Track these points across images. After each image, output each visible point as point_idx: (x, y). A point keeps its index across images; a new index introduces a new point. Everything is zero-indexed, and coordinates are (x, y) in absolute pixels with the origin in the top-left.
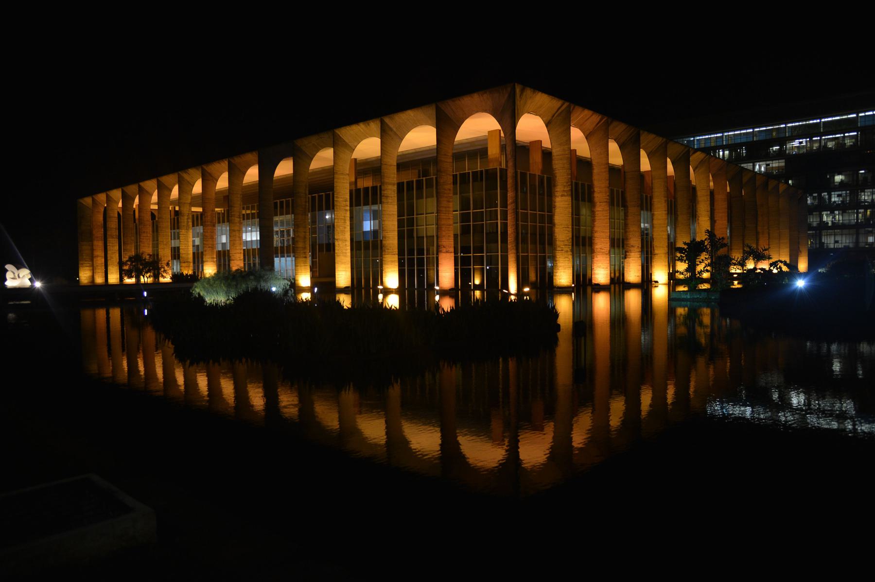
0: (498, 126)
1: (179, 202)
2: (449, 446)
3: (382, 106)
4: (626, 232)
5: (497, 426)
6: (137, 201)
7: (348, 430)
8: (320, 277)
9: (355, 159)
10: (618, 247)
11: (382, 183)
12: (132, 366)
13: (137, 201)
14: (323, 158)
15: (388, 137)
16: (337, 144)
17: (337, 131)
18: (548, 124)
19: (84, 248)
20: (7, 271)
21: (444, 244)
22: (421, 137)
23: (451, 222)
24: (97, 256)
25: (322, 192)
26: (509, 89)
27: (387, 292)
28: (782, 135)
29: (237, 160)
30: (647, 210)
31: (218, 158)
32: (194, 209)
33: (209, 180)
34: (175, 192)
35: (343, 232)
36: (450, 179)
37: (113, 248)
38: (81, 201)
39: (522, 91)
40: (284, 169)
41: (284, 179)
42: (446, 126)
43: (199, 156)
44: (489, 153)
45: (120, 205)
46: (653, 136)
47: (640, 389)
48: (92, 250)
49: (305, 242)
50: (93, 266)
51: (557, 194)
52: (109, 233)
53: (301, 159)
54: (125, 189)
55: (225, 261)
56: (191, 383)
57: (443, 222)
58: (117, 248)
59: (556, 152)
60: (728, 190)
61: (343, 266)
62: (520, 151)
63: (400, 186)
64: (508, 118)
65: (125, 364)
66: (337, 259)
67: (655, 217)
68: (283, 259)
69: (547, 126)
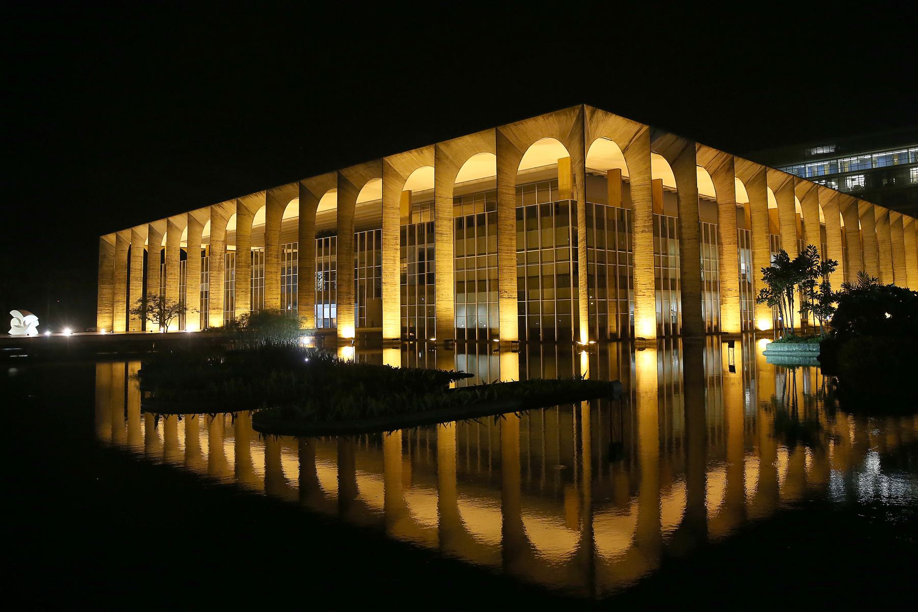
0: (566, 154)
1: (211, 240)
3: (434, 128)
4: (721, 273)
5: (571, 505)
7: (395, 510)
9: (410, 191)
10: (666, 288)
11: (437, 218)
16: (384, 173)
17: (387, 159)
19: (104, 291)
21: (506, 288)
22: (478, 165)
23: (514, 263)
25: (370, 231)
26: (577, 111)
28: (904, 162)
29: (277, 192)
30: (748, 247)
33: (308, 203)
34: (207, 231)
35: (393, 274)
36: (513, 214)
38: (103, 237)
39: (593, 113)
41: (326, 215)
42: (508, 153)
43: (234, 188)
44: (560, 184)
45: (147, 243)
46: (750, 163)
47: (744, 463)
48: (114, 294)
49: (349, 286)
51: (638, 230)
53: (347, 192)
55: (412, 302)
56: (216, 452)
57: (505, 263)
59: (634, 182)
60: (842, 224)
62: (594, 181)
63: (459, 223)
64: (579, 141)
65: (143, 428)
67: (756, 256)
68: (320, 306)
69: (623, 152)
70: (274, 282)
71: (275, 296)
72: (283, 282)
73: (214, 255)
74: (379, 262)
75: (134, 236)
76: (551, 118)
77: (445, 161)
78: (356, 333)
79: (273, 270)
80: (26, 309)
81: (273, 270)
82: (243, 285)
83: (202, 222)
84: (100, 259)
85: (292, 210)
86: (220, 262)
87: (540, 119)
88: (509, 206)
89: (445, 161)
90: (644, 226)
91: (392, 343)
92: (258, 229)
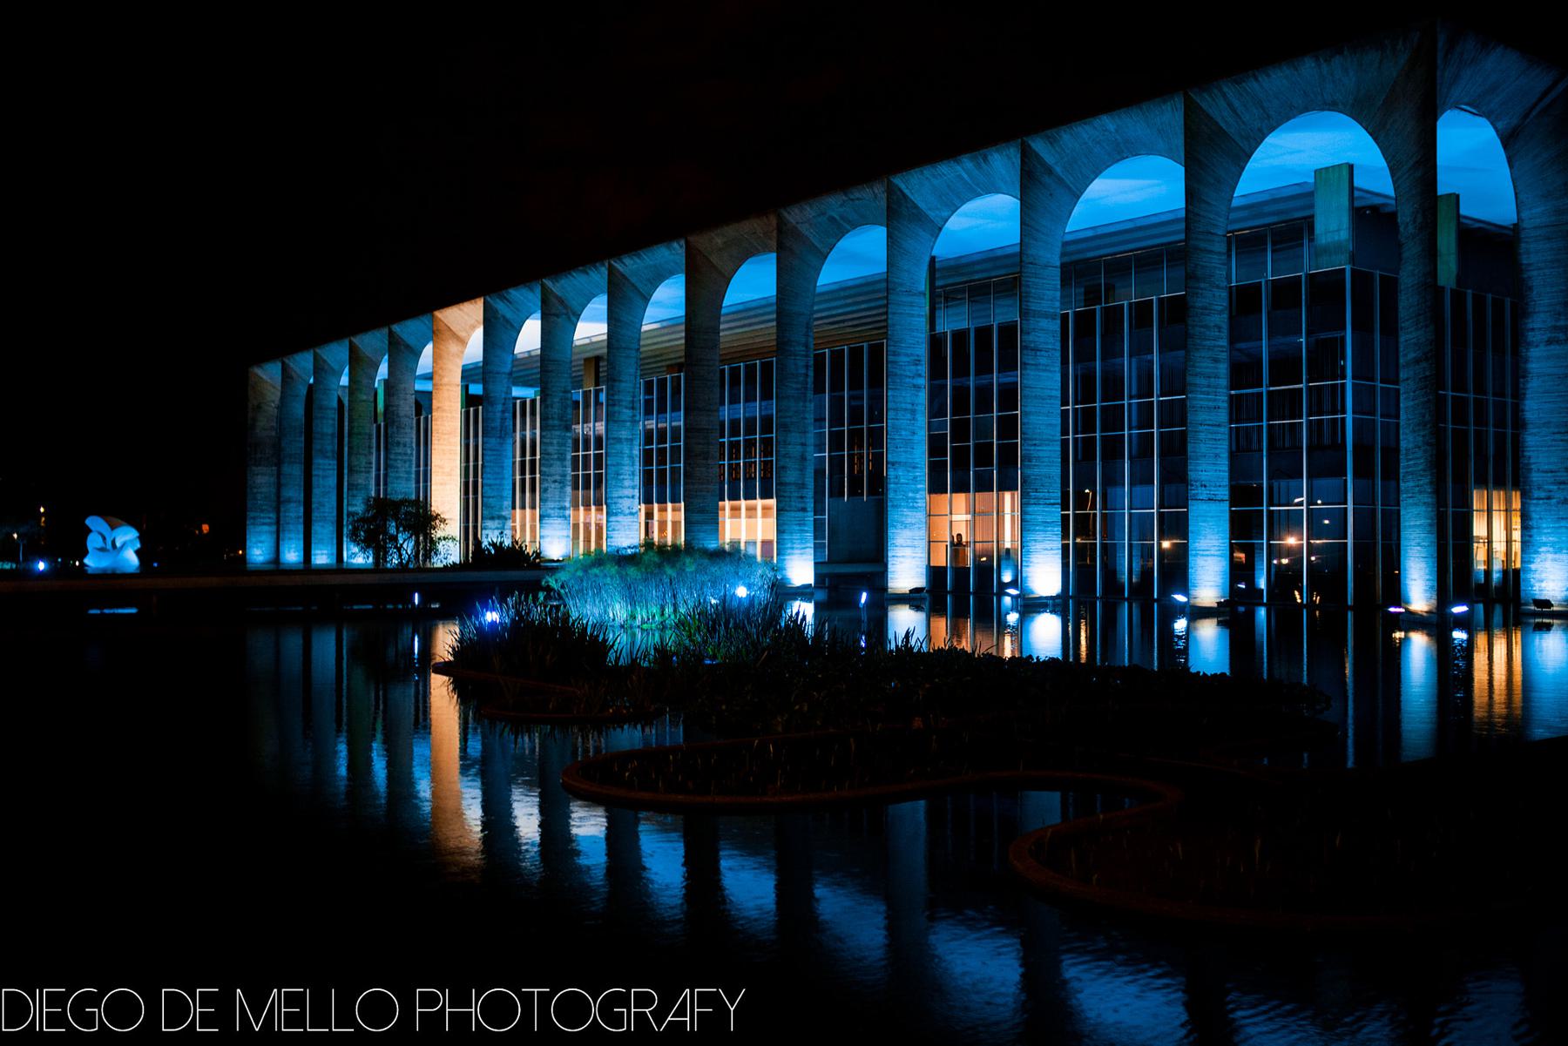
2: (1044, 996)
3: (1023, 104)
6: (383, 371)
8: (831, 561)
12: (359, 765)
13: (383, 371)
14: (857, 255)
15: (1039, 190)
17: (438, 314)
18: (1509, 140)
19: (262, 480)
20: (89, 531)
21: (1204, 476)
22: (1133, 190)
23: (1223, 416)
24: (289, 501)
27: (1031, 606)
31: (523, 278)
32: (517, 392)
33: (558, 320)
35: (909, 443)
37: (325, 480)
38: (258, 371)
40: (753, 283)
41: (747, 312)
42: (1210, 156)
44: (1319, 228)
45: (345, 380)
49: (802, 470)
50: (278, 523)
52: (316, 446)
54: (356, 340)
58: (333, 481)
61: (907, 533)
63: (1244, 301)
66: (893, 515)
69: (1505, 146)
70: (626, 461)
71: (628, 492)
72: (647, 457)
73: (492, 404)
74: (877, 414)
75: (320, 368)
76: (1337, 61)
77: (1047, 179)
78: (817, 575)
79: (624, 434)
80: (117, 515)
81: (624, 434)
82: (556, 469)
83: (462, 334)
84: (250, 415)
85: (529, 337)
86: (503, 419)
87: (928, 171)
88: (1223, 275)
89: (1047, 179)
90: (1555, 328)
91: (803, 593)
92: (530, 357)
